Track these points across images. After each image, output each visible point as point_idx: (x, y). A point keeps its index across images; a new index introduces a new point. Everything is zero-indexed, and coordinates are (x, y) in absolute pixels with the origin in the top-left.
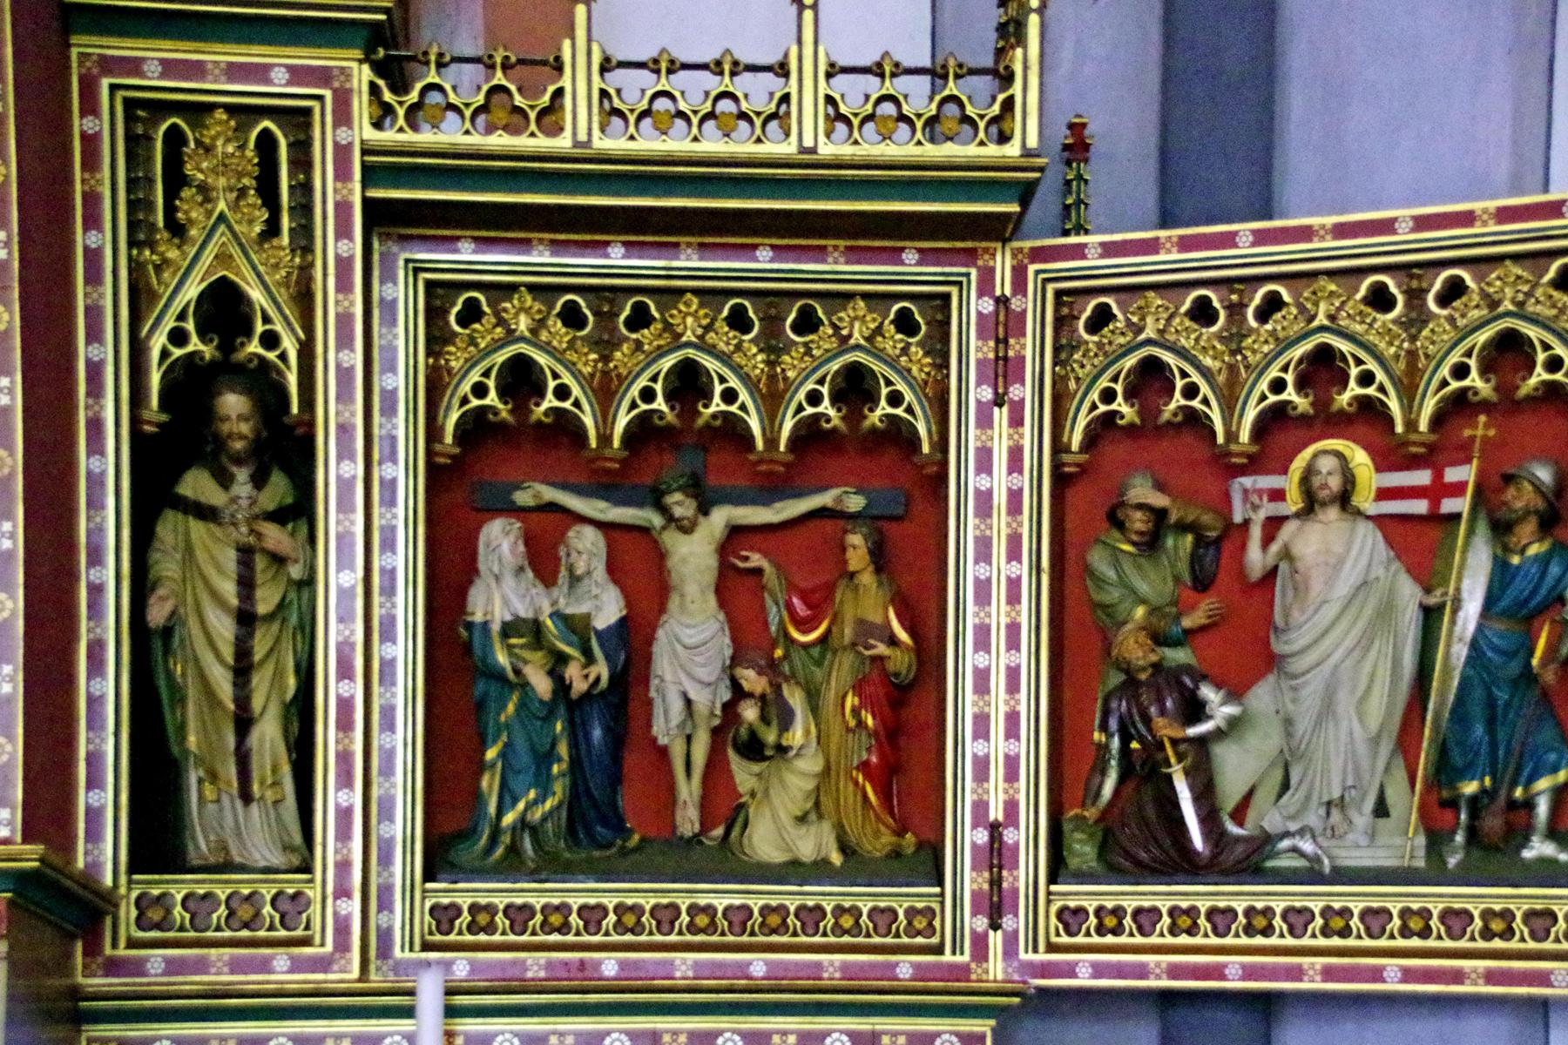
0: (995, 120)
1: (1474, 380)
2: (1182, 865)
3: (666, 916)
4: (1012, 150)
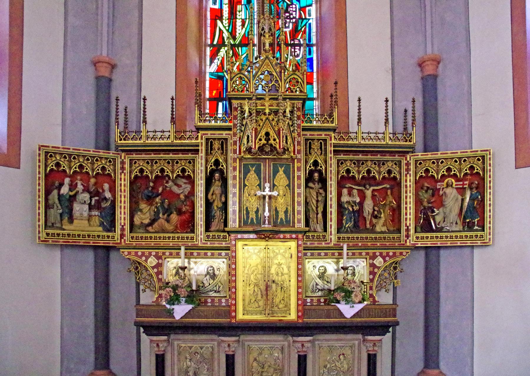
1: (468, 171)
2: (432, 231)
3: (367, 238)
4: (412, 143)
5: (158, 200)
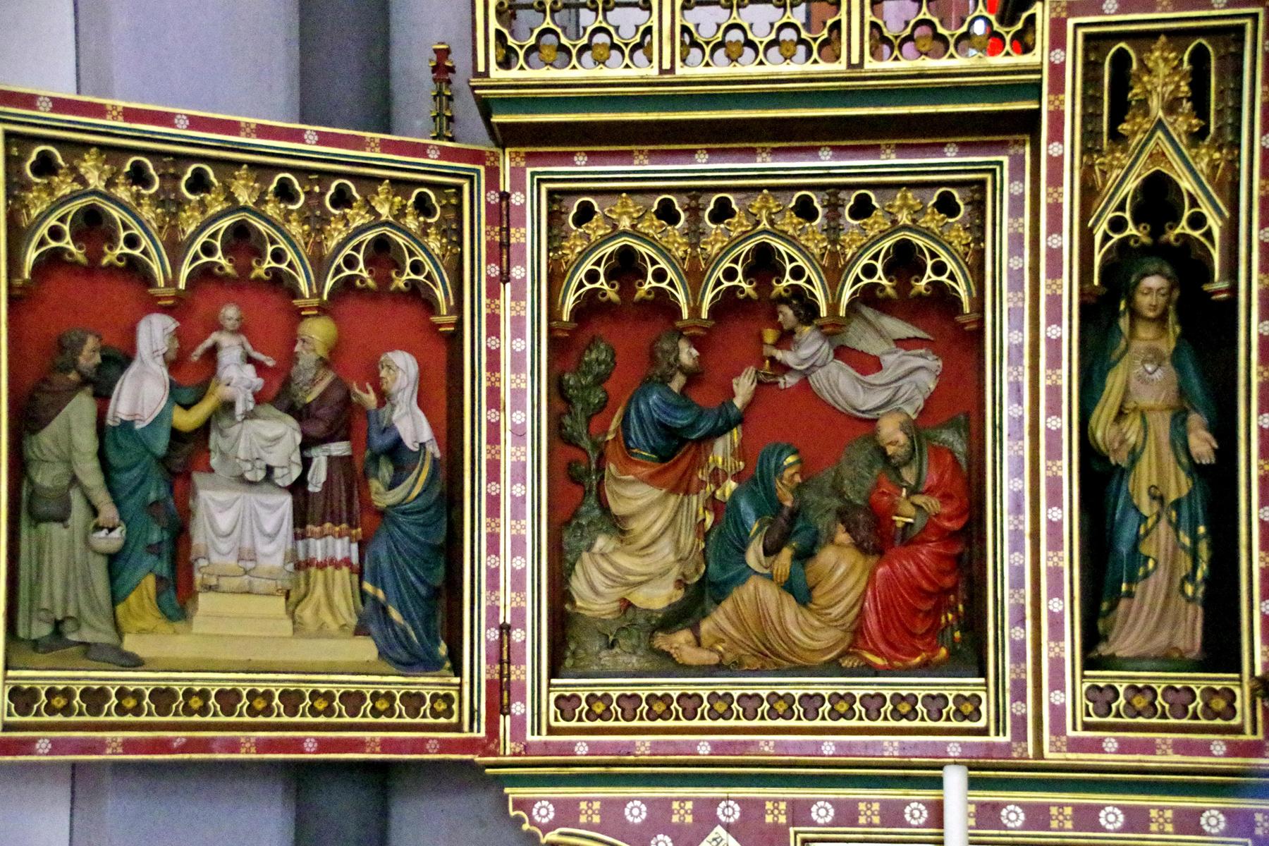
0: (825, 43)
3: (873, 704)
5: (721, 452)
